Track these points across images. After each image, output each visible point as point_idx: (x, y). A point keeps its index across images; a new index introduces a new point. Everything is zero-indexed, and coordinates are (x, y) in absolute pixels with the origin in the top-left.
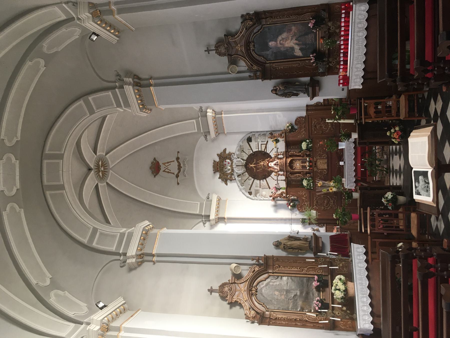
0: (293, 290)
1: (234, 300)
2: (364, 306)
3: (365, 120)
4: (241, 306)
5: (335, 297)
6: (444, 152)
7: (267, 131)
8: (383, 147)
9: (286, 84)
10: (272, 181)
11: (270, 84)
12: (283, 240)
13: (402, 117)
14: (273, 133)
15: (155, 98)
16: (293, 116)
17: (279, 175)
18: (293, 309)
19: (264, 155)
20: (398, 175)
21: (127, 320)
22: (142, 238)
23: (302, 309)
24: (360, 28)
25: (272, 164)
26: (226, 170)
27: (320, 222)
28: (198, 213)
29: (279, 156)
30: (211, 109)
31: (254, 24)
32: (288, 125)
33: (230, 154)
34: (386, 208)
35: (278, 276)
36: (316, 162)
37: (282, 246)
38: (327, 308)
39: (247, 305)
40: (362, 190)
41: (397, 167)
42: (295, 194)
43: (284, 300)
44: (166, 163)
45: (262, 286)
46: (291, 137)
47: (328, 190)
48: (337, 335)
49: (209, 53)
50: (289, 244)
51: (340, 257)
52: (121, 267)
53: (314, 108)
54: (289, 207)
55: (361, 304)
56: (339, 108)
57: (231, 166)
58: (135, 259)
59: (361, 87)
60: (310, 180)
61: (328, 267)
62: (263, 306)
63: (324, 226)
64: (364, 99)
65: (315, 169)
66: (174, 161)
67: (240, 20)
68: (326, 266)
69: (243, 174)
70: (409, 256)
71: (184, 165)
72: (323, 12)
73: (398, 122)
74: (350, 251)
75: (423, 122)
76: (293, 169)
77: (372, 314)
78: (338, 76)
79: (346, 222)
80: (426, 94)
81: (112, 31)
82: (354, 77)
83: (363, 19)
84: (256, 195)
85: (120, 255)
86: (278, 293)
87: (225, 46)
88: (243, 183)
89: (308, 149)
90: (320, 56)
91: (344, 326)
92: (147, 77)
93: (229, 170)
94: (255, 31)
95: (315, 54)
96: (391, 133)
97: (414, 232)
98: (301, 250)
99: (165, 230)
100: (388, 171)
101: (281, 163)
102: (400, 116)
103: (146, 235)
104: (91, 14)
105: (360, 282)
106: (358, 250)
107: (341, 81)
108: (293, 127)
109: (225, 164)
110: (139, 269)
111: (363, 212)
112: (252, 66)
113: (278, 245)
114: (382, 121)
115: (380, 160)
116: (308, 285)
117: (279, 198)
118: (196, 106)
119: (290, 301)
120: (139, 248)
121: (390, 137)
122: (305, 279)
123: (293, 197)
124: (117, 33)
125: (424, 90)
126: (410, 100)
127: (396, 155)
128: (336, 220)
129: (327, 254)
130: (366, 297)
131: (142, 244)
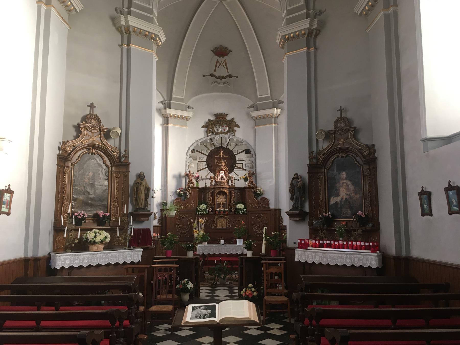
1: (83, 130)
2: (80, 260)
3: (264, 263)
4: (77, 137)
5: (88, 232)
6: (231, 336)
7: (256, 170)
8: (237, 281)
9: (303, 188)
10: (205, 173)
11: (304, 173)
12: (146, 182)
13: (266, 298)
14: (254, 176)
15: (295, 52)
16: (270, 196)
18: (75, 191)
19: (232, 166)
20: (209, 294)
21: (58, 13)
22: (147, 33)
23: (75, 200)
24: (354, 260)
25: (222, 174)
26: (218, 127)
27: (163, 219)
28: (174, 96)
29: (230, 182)
30: (280, 112)
31: (364, 157)
32: (261, 190)
33: (234, 131)
34: (178, 283)
35: (108, 176)
36: (224, 217)
37: (139, 181)
38: (77, 224)
39: (77, 143)
40: (196, 260)
41: (217, 293)
42: (191, 197)
43: (84, 181)
44: (226, 63)
45: (98, 160)
46: (249, 194)
47: (195, 229)
48: (49, 234)
49: (338, 110)
50: (142, 187)
51: (129, 238)
52: (116, 9)
53: (277, 216)
54: (179, 190)
55: (81, 257)
56: (277, 240)
57: (222, 133)
58: (124, 24)
59: (296, 260)
60: (206, 211)
61: (119, 226)
62: (77, 160)
63: (160, 224)
64: (285, 263)
65: (216, 217)
66: (228, 72)
67: (369, 143)
68: (120, 224)
69: (213, 144)
70: (130, 302)
71: (224, 83)
72: (371, 224)
73: (261, 294)
74: (134, 248)
75: (262, 318)
76: (217, 194)
77: (72, 268)
78: (308, 238)
79: (163, 244)
80: (287, 320)
81: (367, 8)
82: (307, 254)
83: (362, 262)
85: (129, 8)
86: (91, 175)
87: (345, 127)
88: (203, 144)
89: (237, 210)
90: (329, 221)
91: (59, 241)
92: (317, 44)
94: (357, 158)
95: (331, 216)
96: (251, 288)
97: (154, 308)
98: (136, 200)
99: (155, 59)
100: (214, 286)
101: (224, 183)
102: (267, 296)
103: (150, 37)
105: (104, 257)
106: (136, 256)
107: (303, 242)
108: (259, 195)
109: (223, 126)
110: (113, 28)
111: (174, 261)
112: (323, 155)
113: (140, 176)
114: (263, 279)
115: (224, 278)
116: (100, 206)
117: (188, 180)
118: (284, 97)
119: (83, 188)
120: (136, 29)
121: (247, 287)
122: (106, 203)
123: (188, 194)
124: (364, 13)
125: (292, 319)
126: (282, 305)
127: (229, 293)
128: (166, 235)
129: (131, 226)
130: (89, 262)
131: (140, 33)
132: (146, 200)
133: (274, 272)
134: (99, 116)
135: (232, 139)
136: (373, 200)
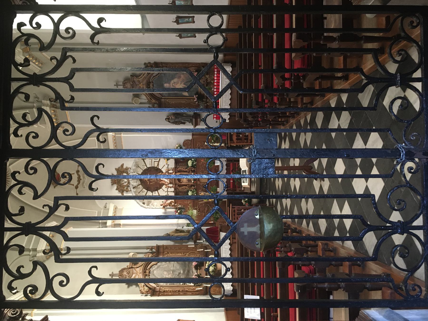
0: (178, 269)
17: (169, 187)
19: (156, 170)
26: (123, 182)
29: (170, 172)
32: (177, 146)
33: (127, 169)
50: (177, 237)
61: (204, 250)
81: (37, 63)
84: (148, 205)
89: (193, 166)
93: (125, 182)
95: (197, 96)
104: (22, 50)
117: (168, 206)
123: (180, 206)
132: (185, 232)
133: (236, 138)
134: (120, 269)
135: (133, 170)
136: (184, 67)
